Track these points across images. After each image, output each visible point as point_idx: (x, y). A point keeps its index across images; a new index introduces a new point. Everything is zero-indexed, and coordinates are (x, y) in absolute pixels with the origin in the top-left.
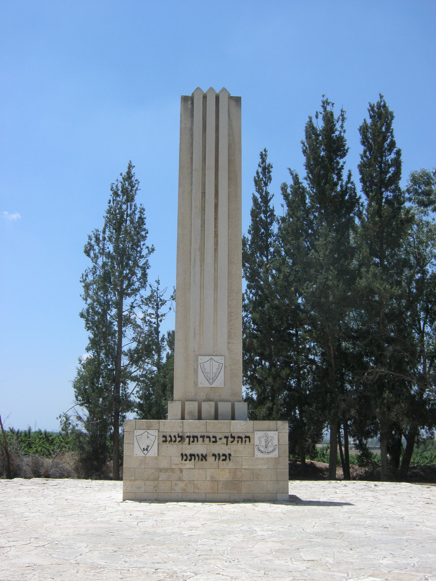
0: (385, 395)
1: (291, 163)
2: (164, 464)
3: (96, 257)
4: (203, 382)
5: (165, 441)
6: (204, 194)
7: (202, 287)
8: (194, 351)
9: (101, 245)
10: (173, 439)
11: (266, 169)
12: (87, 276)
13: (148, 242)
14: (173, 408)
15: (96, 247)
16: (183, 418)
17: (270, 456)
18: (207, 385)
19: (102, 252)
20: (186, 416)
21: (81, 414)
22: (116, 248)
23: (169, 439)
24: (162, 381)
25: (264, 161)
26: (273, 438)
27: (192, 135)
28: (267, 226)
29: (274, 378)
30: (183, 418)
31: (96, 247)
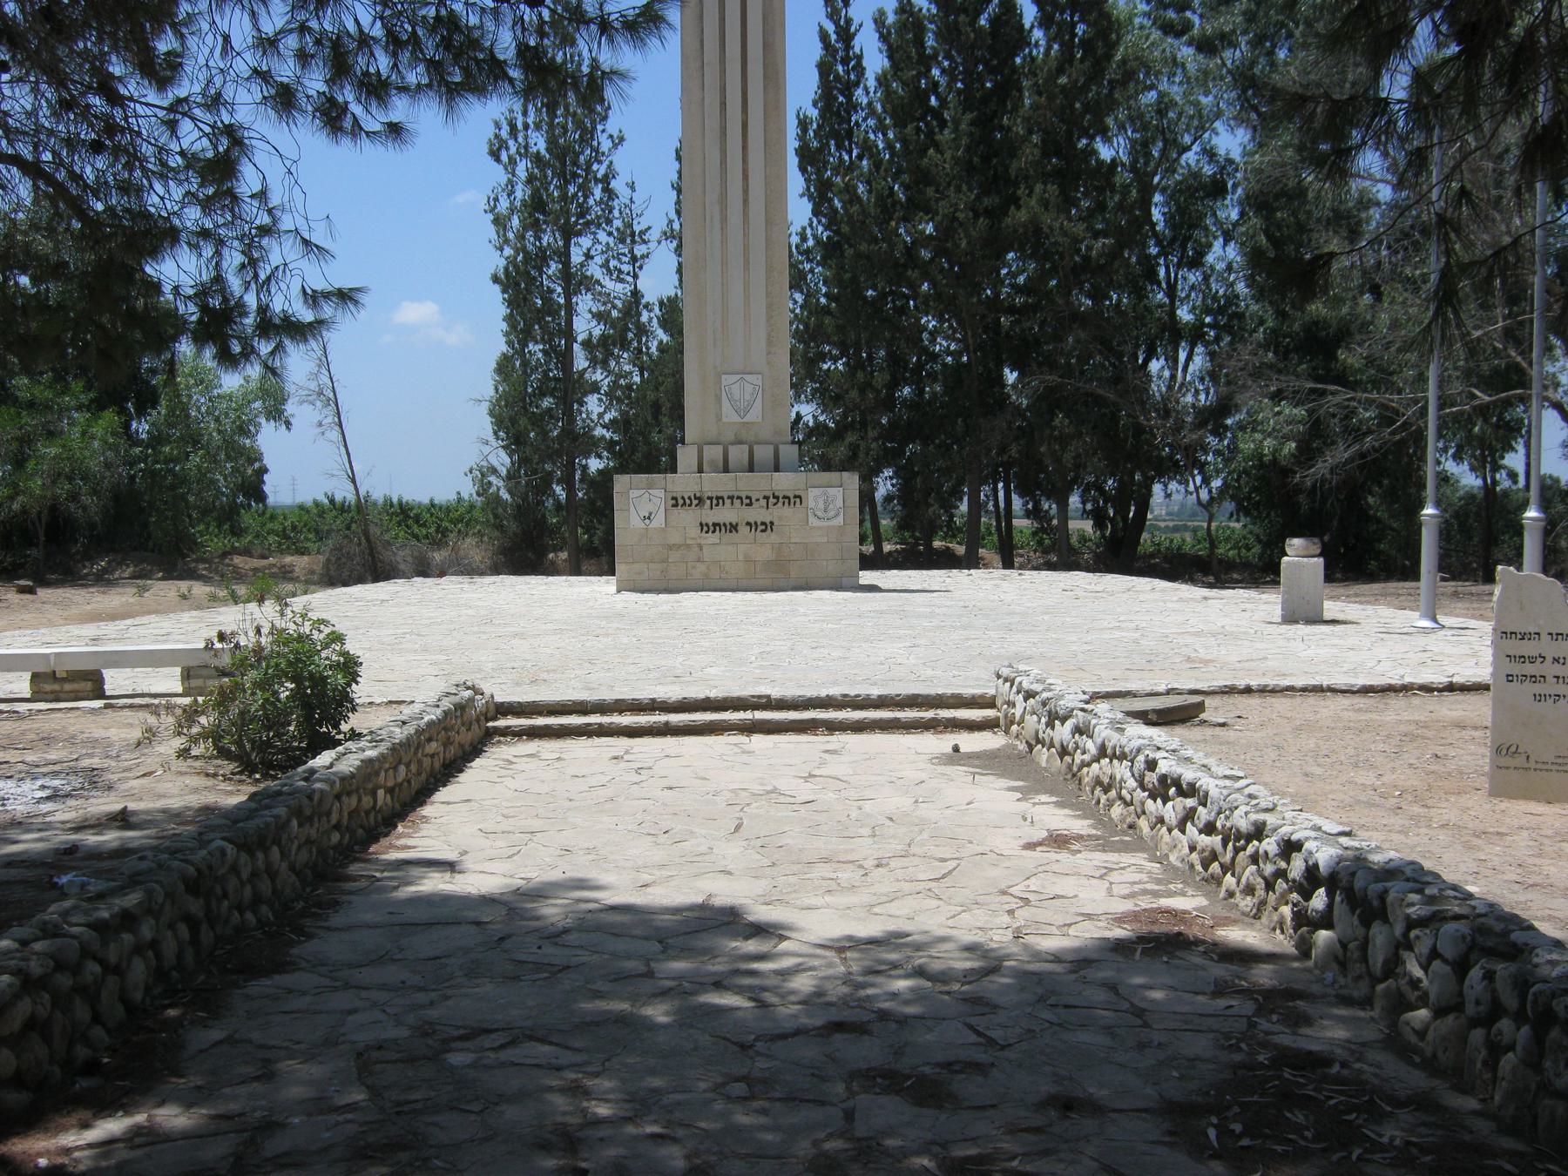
0: (1057, 422)
2: (675, 538)
3: (512, 161)
4: (729, 415)
5: (675, 505)
6: (723, 104)
9: (520, 140)
12: (496, 199)
13: (612, 126)
14: (686, 456)
15: (511, 143)
16: (700, 471)
18: (736, 419)
19: (525, 151)
20: (705, 468)
21: (496, 464)
22: (552, 143)
24: (651, 396)
28: (848, 88)
29: (862, 391)
30: (700, 471)
31: (511, 143)
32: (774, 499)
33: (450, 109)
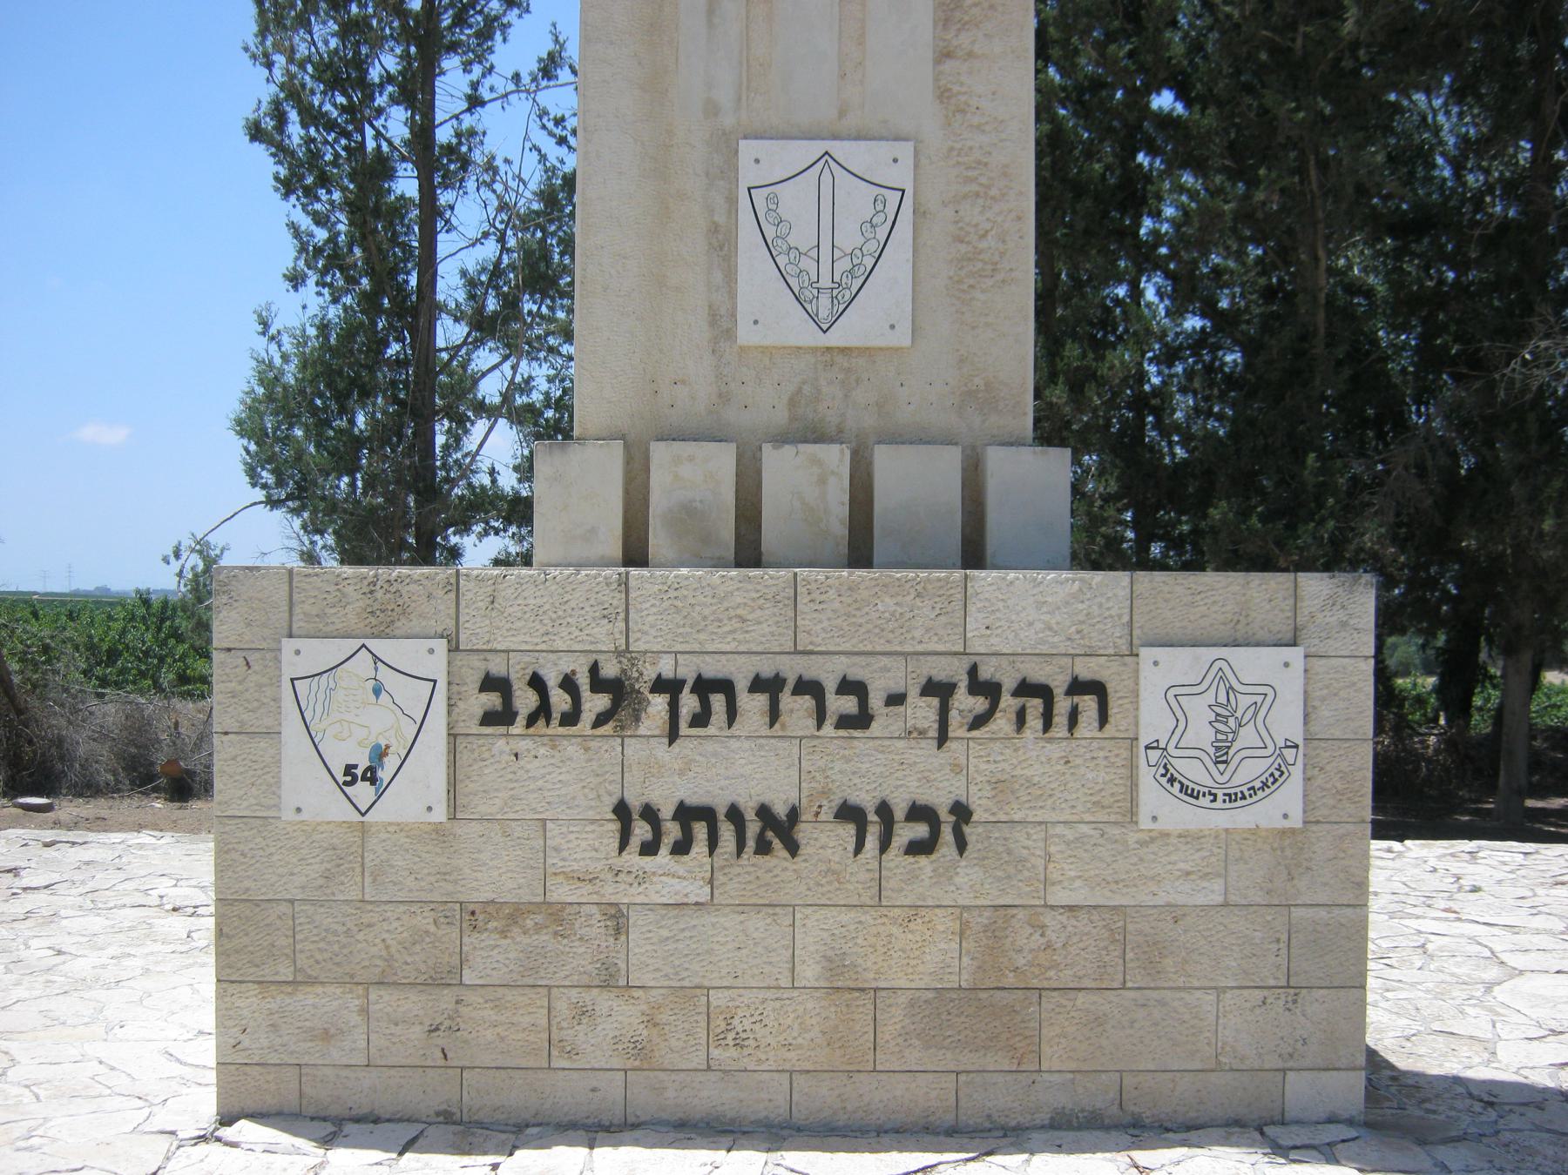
2: (496, 874)
8: (712, 109)
10: (560, 700)
18: (798, 331)
23: (526, 700)
26: (1267, 693)
32: (977, 695)
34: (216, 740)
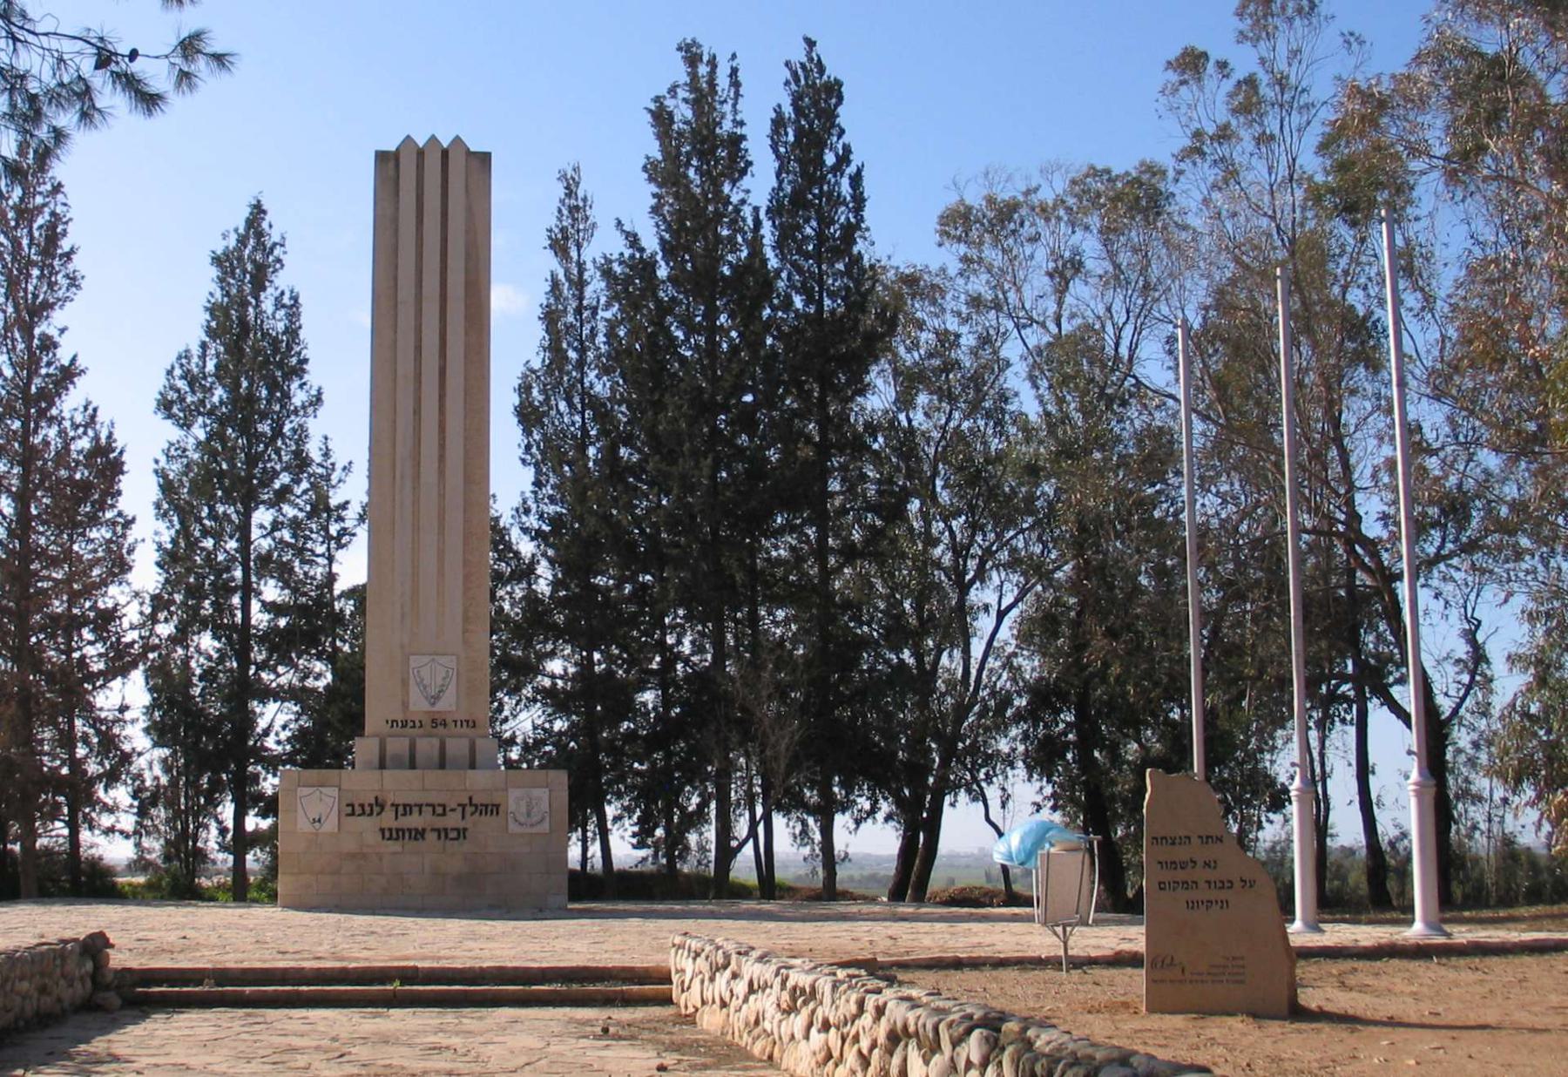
1: (627, 212)
5: (353, 814)
6: (418, 349)
7: (416, 528)
8: (402, 647)
10: (367, 809)
11: (575, 209)
14: (364, 748)
17: (534, 830)
20: (388, 763)
23: (358, 810)
25: (570, 192)
27: (396, 231)
33: (149, 110)
34: (1049, 290)
